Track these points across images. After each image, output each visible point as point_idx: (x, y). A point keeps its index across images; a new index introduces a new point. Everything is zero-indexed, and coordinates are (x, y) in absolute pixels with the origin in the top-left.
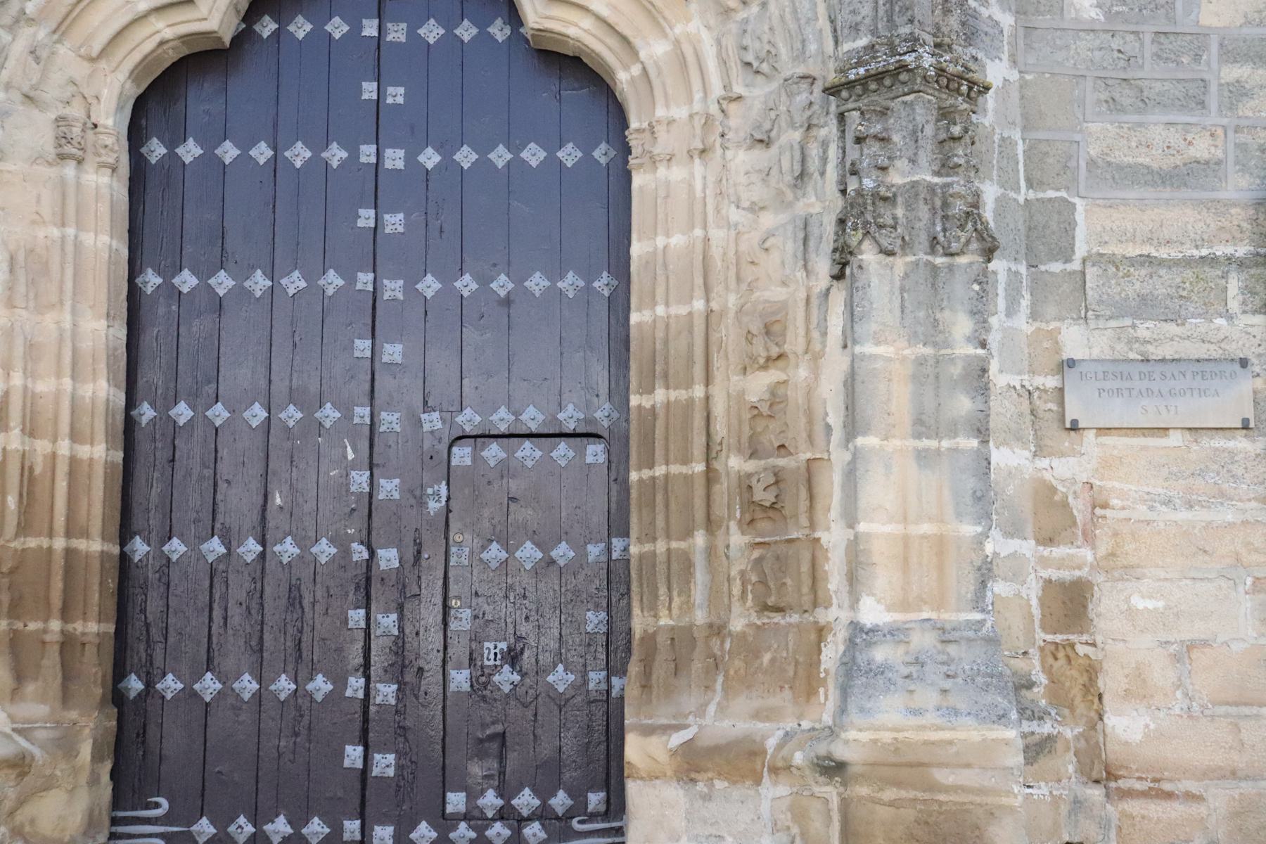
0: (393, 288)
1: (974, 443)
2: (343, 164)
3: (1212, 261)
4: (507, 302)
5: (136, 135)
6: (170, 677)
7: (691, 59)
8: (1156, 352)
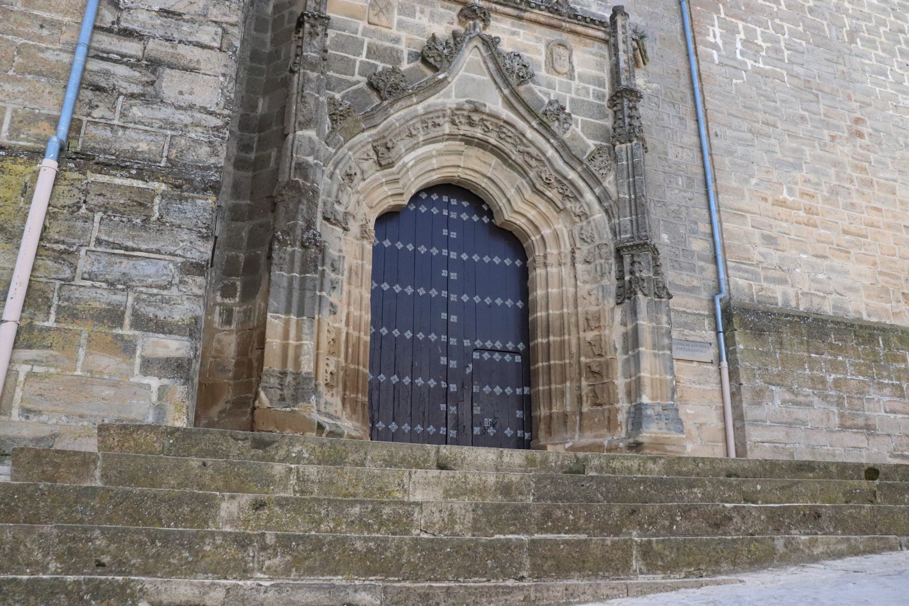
0: (453, 298)
1: (669, 352)
2: (437, 254)
4: (490, 306)
8: (688, 338)
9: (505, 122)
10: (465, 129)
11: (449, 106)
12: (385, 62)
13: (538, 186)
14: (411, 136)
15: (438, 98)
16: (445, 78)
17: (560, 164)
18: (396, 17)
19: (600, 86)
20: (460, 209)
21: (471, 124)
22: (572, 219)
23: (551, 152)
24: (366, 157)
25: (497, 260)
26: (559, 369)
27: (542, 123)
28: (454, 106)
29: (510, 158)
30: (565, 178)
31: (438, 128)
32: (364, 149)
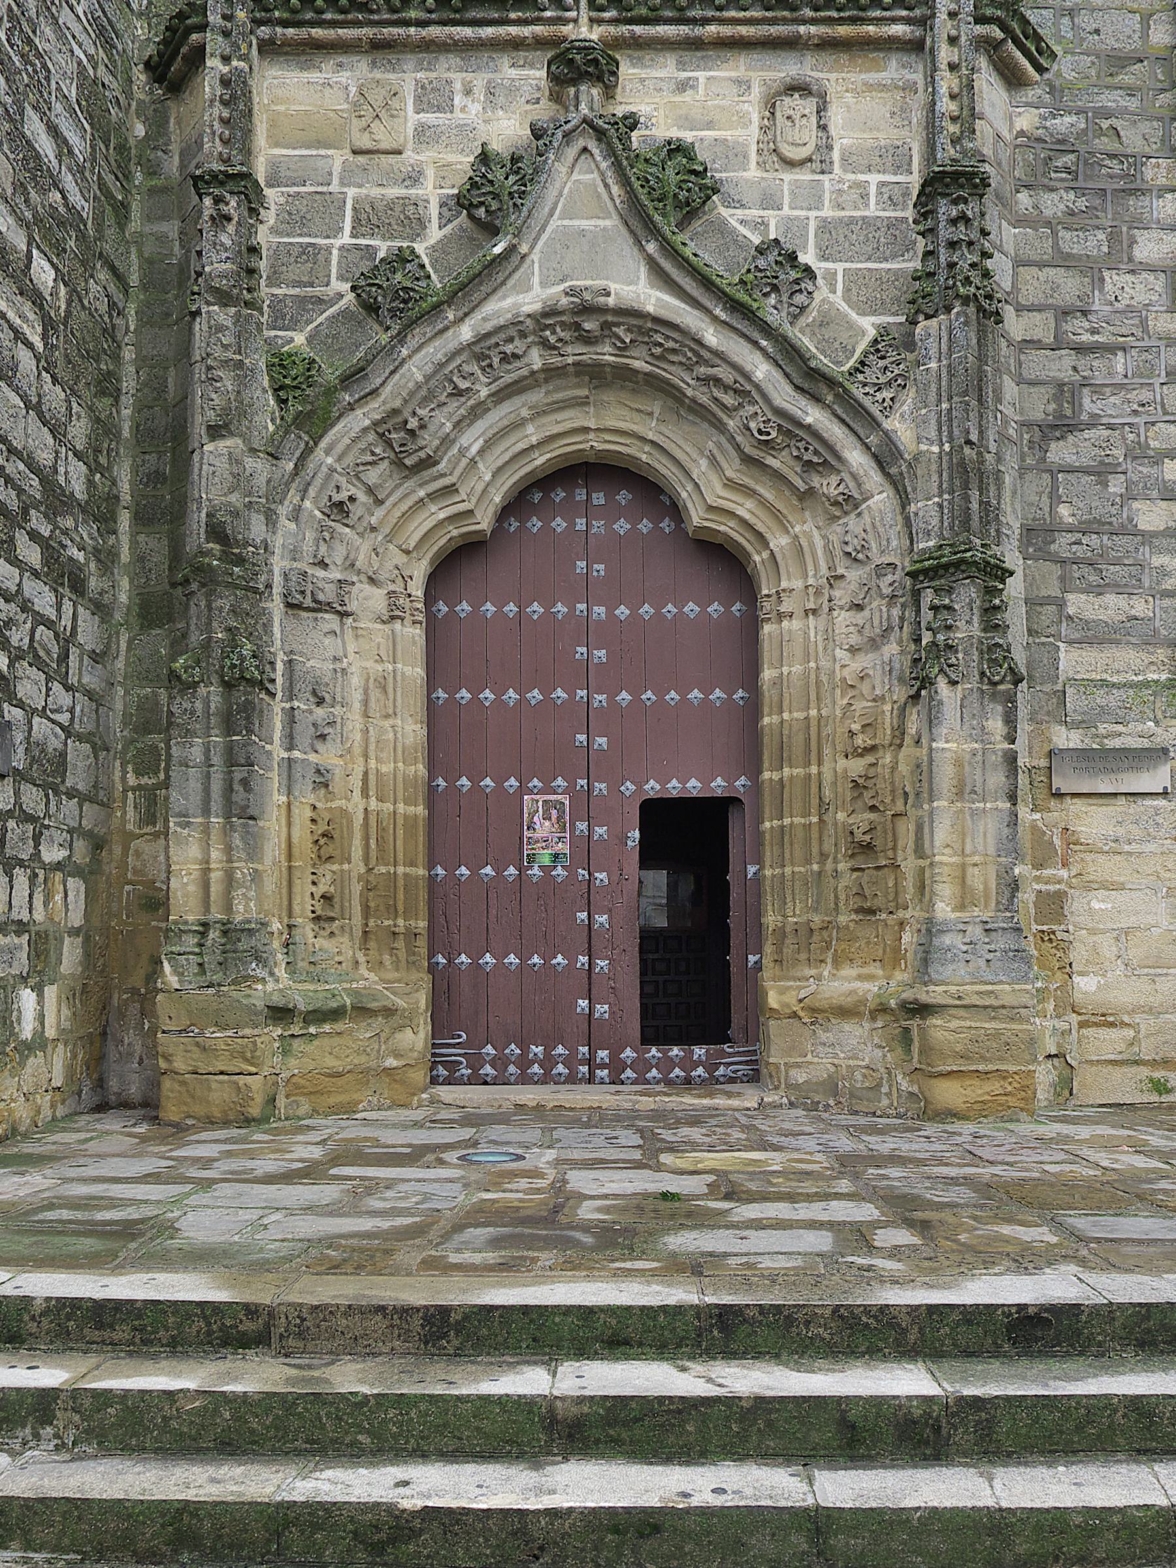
3: (1146, 684)
5: (430, 598)
6: (463, 956)
7: (806, 549)
9: (656, 320)
10: (574, 353)
11: (527, 309)
12: (392, 237)
13: (748, 450)
14: (458, 393)
15: (504, 297)
16: (511, 250)
17: (784, 395)
18: (413, 118)
19: (897, 169)
20: (611, 512)
21: (588, 339)
22: (826, 512)
23: (761, 370)
24: (370, 458)
25: (691, 608)
26: (800, 834)
27: (735, 306)
28: (537, 307)
29: (685, 395)
30: (799, 424)
31: (518, 364)
32: (362, 445)
